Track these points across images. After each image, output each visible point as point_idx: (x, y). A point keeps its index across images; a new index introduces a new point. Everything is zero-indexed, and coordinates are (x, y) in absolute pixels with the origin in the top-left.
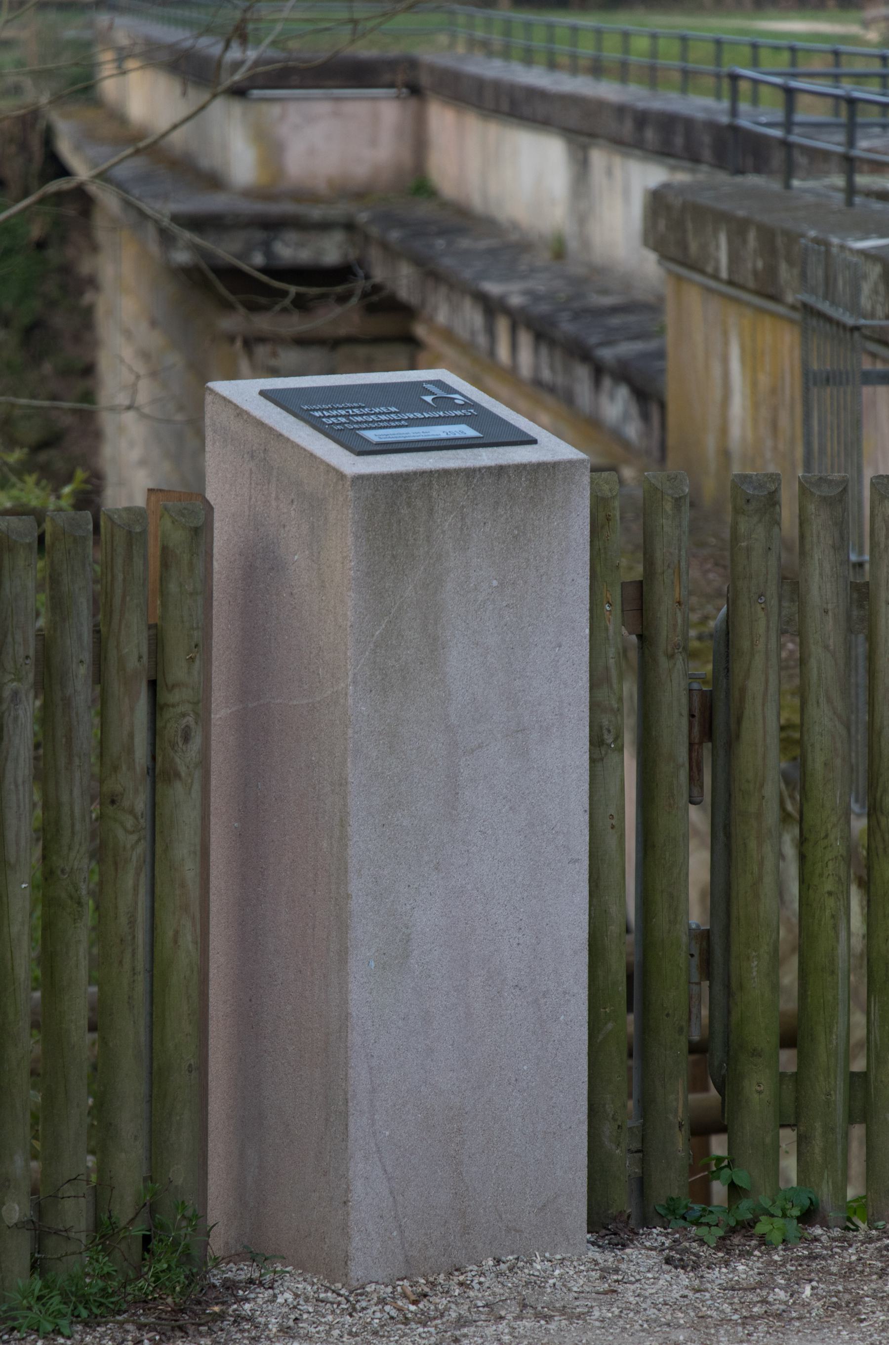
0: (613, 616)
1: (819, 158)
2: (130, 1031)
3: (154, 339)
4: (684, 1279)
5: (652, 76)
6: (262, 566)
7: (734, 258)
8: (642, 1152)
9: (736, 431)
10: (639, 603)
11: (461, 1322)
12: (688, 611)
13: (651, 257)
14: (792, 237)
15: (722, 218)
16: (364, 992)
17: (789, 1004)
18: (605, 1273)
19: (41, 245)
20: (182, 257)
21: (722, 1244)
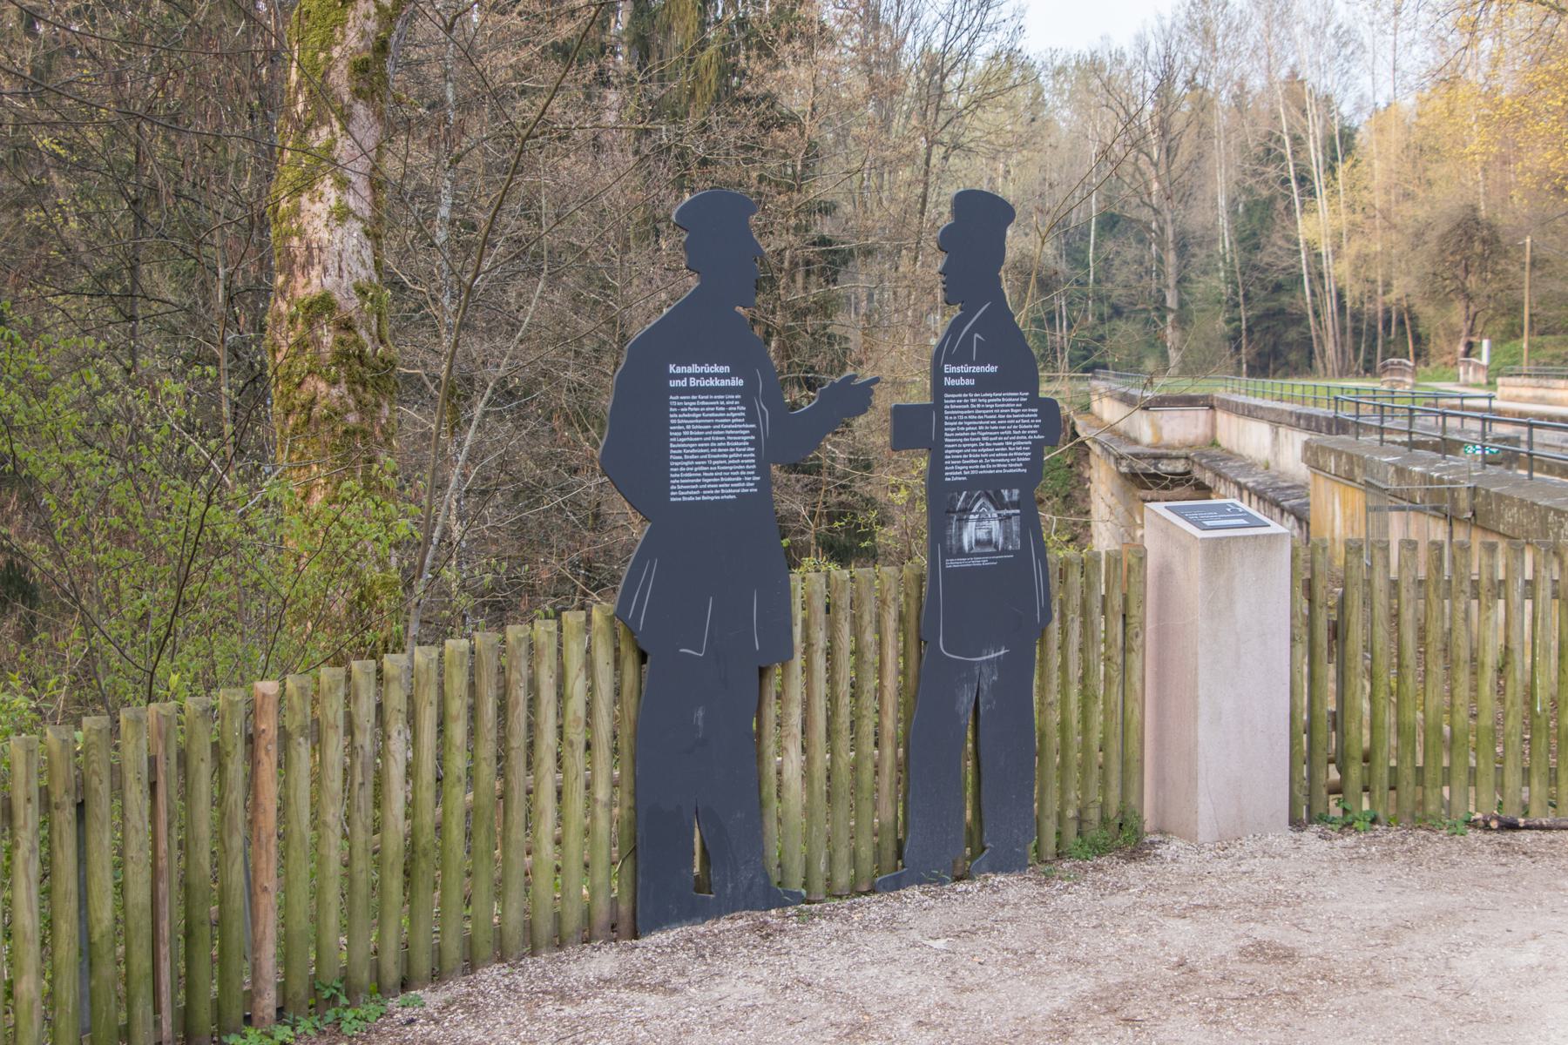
0: (1299, 592)
1: (1368, 429)
2: (1115, 746)
3: (1113, 501)
4: (1326, 844)
5: (1303, 401)
6: (1165, 572)
7: (1337, 466)
8: (1310, 795)
9: (1337, 531)
10: (1309, 587)
11: (1241, 858)
12: (1328, 593)
13: (1304, 466)
14: (1360, 457)
15: (1332, 450)
16: (1205, 733)
17: (1366, 744)
18: (1296, 841)
19: (1070, 466)
20: (1124, 469)
21: (1340, 831)
